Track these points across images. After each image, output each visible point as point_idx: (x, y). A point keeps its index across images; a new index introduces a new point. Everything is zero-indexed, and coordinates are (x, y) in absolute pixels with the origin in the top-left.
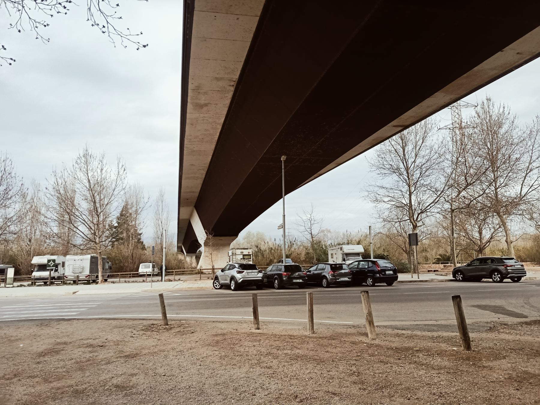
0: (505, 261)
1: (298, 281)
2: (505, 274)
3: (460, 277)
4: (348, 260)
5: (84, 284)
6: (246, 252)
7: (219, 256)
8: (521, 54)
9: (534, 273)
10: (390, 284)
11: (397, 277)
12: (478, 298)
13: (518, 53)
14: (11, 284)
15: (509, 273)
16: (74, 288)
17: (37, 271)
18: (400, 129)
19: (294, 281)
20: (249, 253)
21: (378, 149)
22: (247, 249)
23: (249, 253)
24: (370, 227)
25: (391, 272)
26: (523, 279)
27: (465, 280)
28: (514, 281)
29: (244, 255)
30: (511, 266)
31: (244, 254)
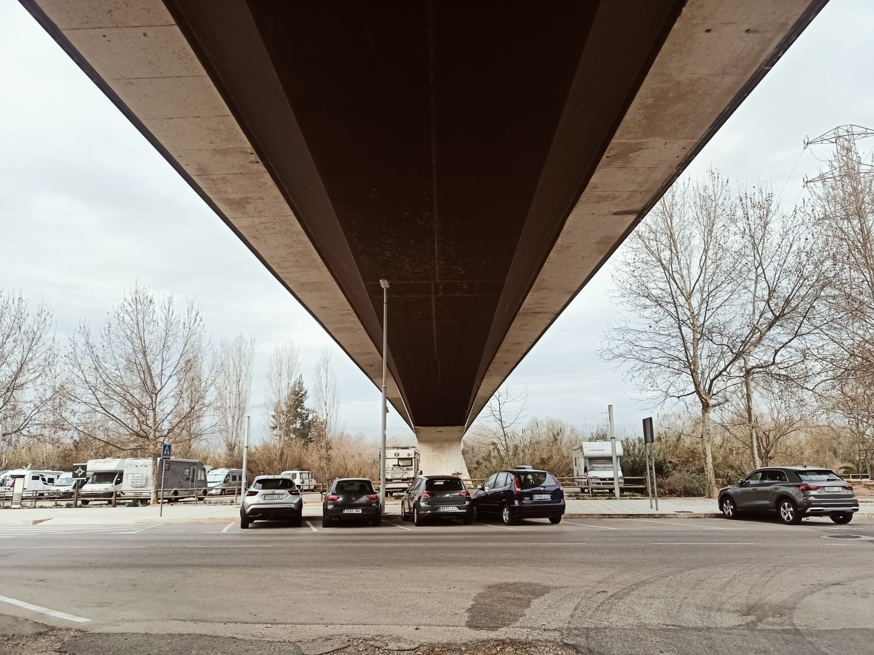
0: (801, 476)
1: (354, 511)
2: (801, 505)
3: (729, 509)
4: (592, 469)
5: (130, 505)
6: (403, 454)
7: (444, 459)
8: (756, 31)
9: (873, 506)
10: (555, 521)
11: (563, 507)
12: (505, 562)
13: (748, 30)
14: (17, 504)
15: (810, 504)
16: (30, 514)
17: (92, 483)
18: (632, 218)
19: (346, 512)
20: (409, 455)
21: (630, 257)
22: (407, 448)
23: (409, 455)
24: (610, 407)
25: (548, 497)
26: (855, 515)
27: (741, 514)
28: (838, 522)
29: (399, 459)
30: (817, 488)
31: (400, 457)
